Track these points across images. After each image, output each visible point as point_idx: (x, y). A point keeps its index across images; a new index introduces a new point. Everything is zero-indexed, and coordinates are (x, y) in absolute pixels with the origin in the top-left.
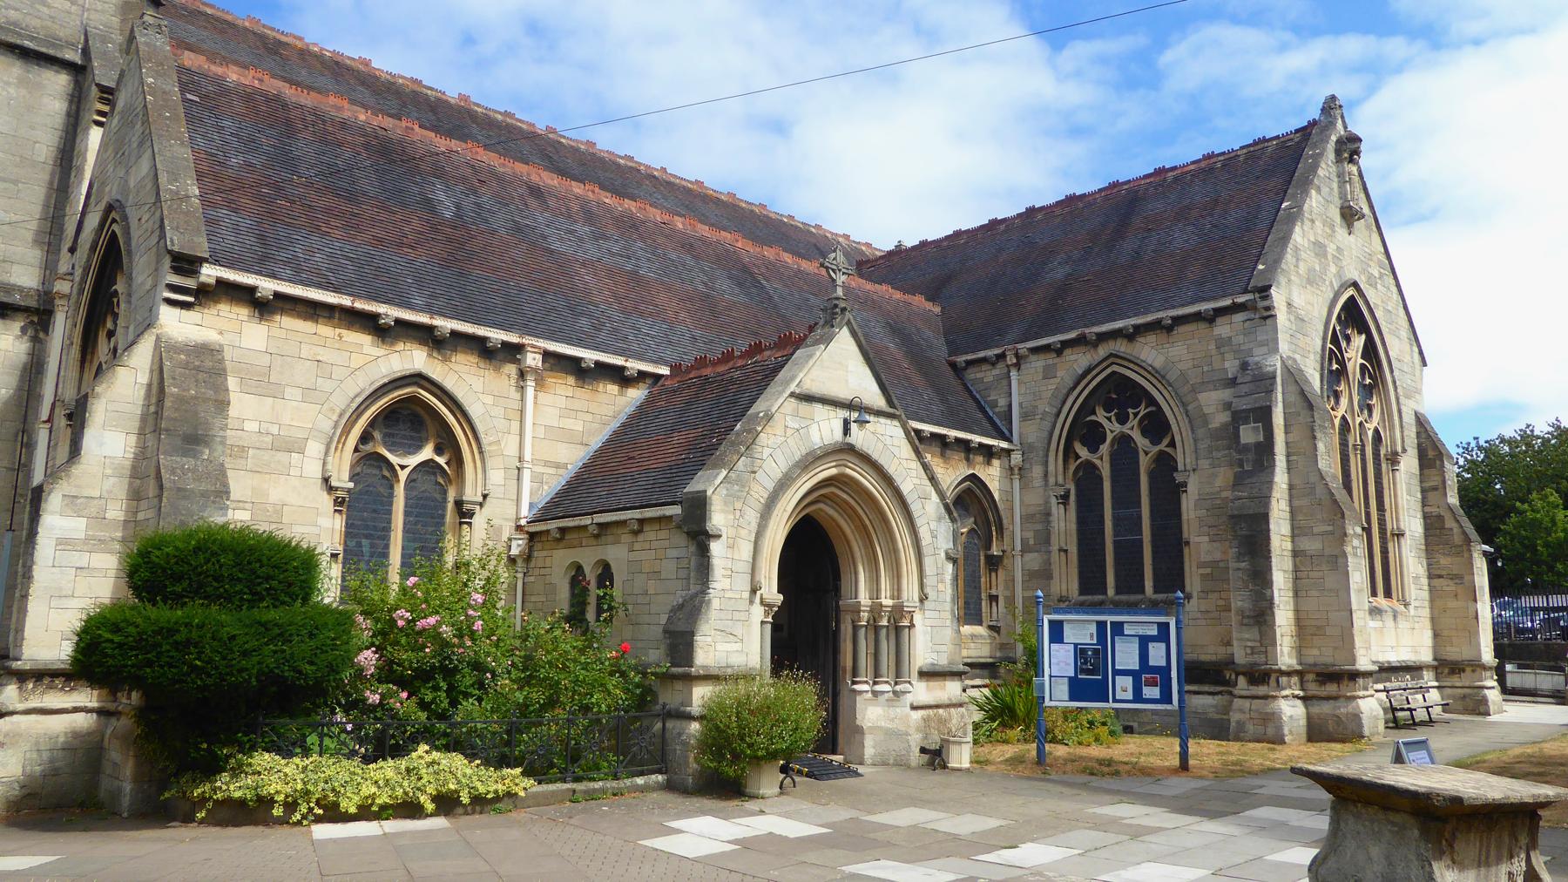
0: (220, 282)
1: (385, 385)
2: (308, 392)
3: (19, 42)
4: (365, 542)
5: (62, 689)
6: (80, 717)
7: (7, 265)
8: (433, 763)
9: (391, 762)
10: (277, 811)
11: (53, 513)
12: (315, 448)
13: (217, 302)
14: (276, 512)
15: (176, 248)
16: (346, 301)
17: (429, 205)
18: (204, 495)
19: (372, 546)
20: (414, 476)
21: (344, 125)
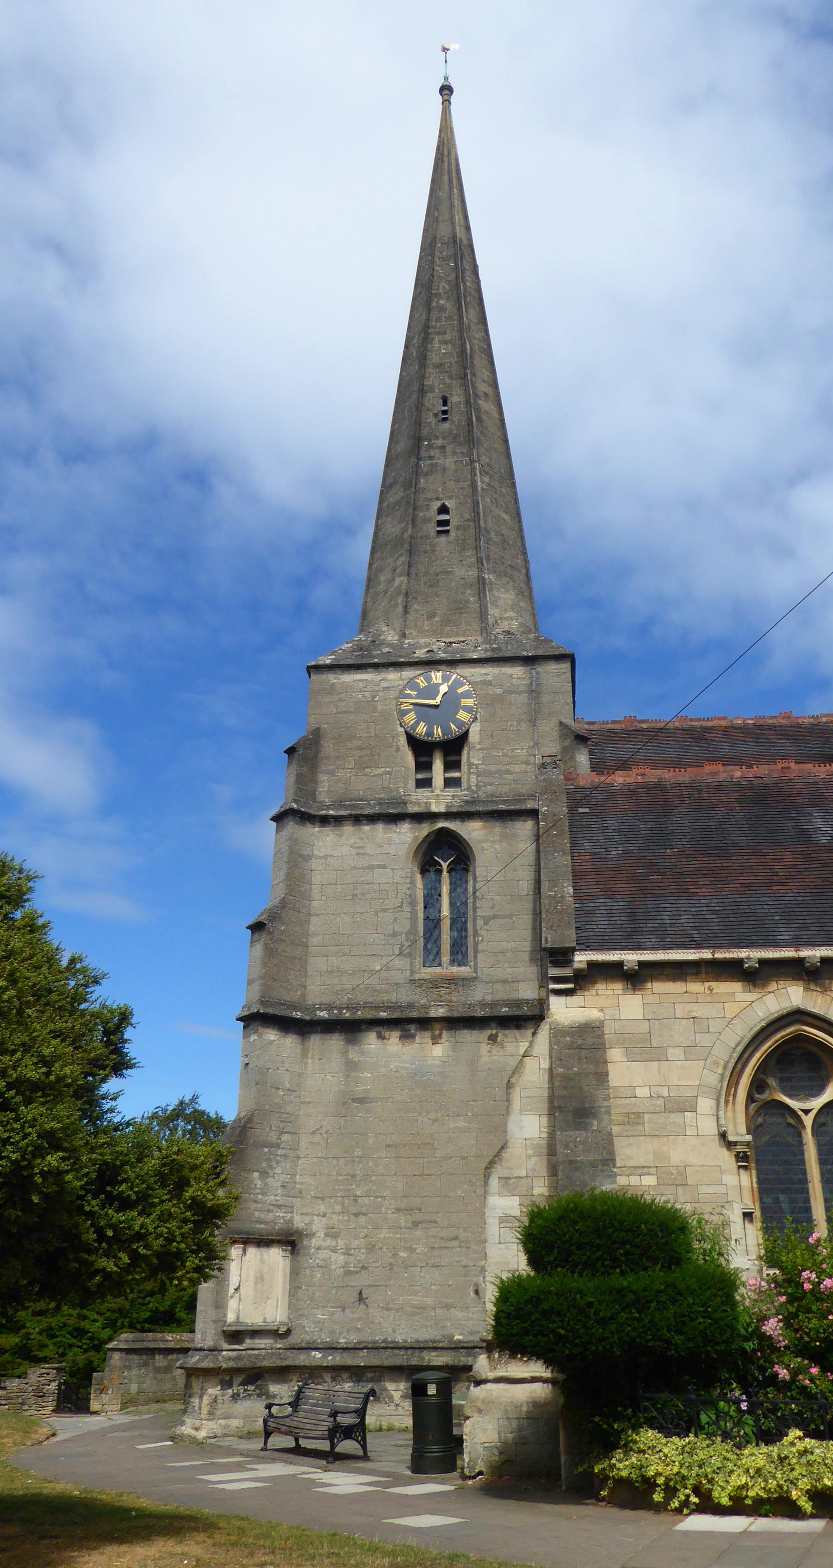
0: (591, 964)
1: (763, 1030)
2: (690, 1051)
3: (495, 808)
4: (782, 1197)
5: (521, 1359)
6: (538, 1386)
7: (515, 984)
8: (805, 1452)
9: (764, 1449)
10: (658, 1497)
11: (493, 1194)
12: (706, 1104)
13: (594, 983)
14: (680, 1174)
15: (549, 945)
16: (706, 954)
17: (805, 836)
18: (593, 1164)
19: (792, 1201)
20: (822, 1119)
21: (720, 787)
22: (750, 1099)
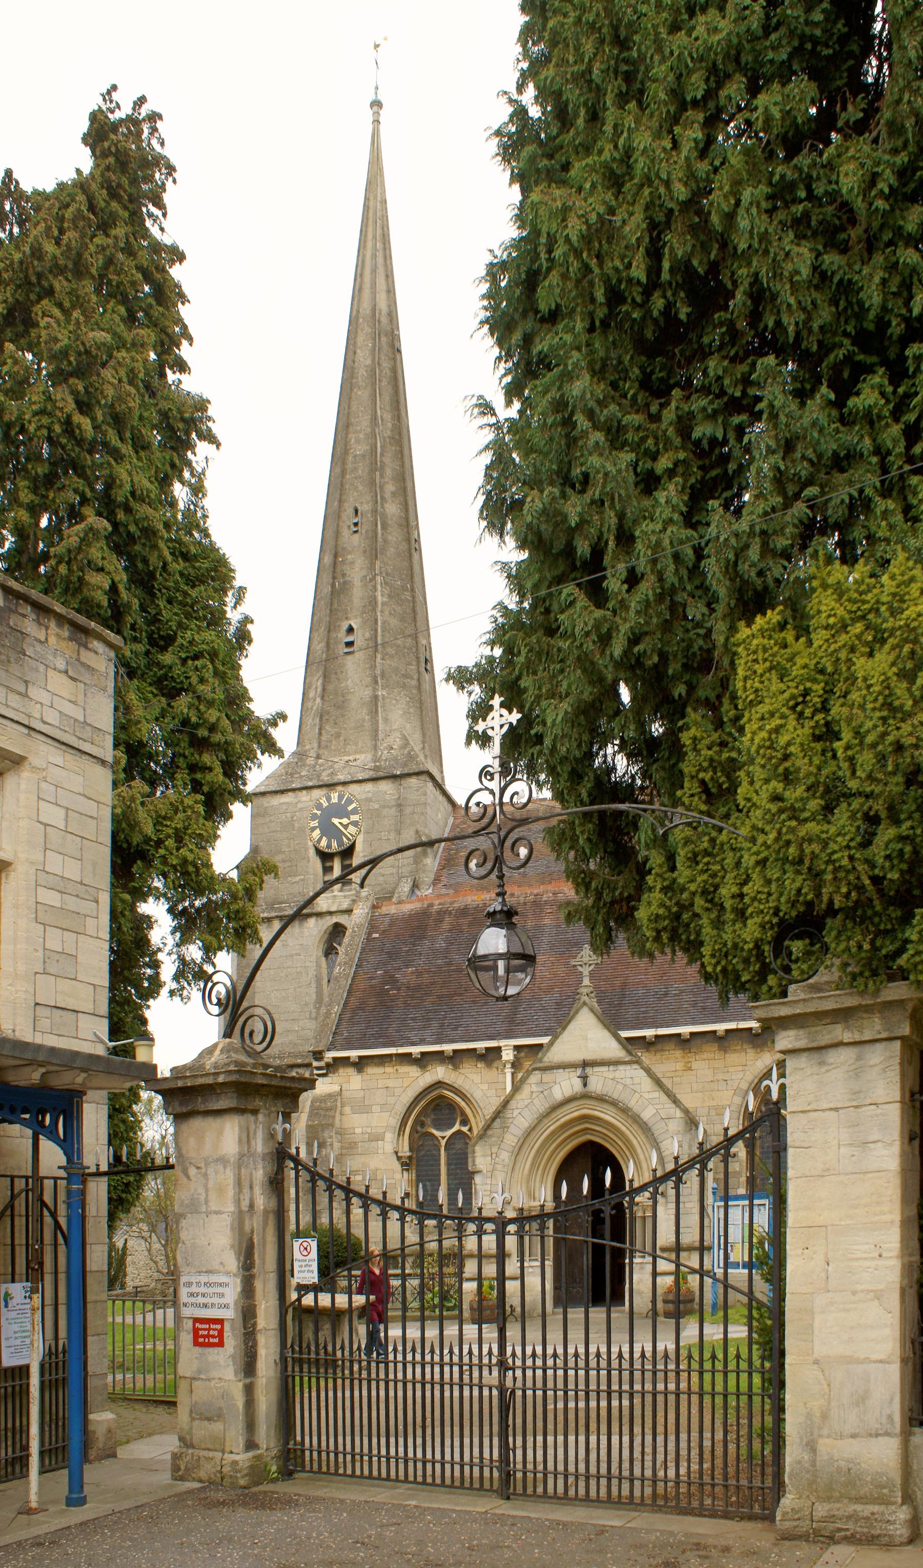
0: (335, 1059)
12: (390, 1136)
22: (414, 1130)
